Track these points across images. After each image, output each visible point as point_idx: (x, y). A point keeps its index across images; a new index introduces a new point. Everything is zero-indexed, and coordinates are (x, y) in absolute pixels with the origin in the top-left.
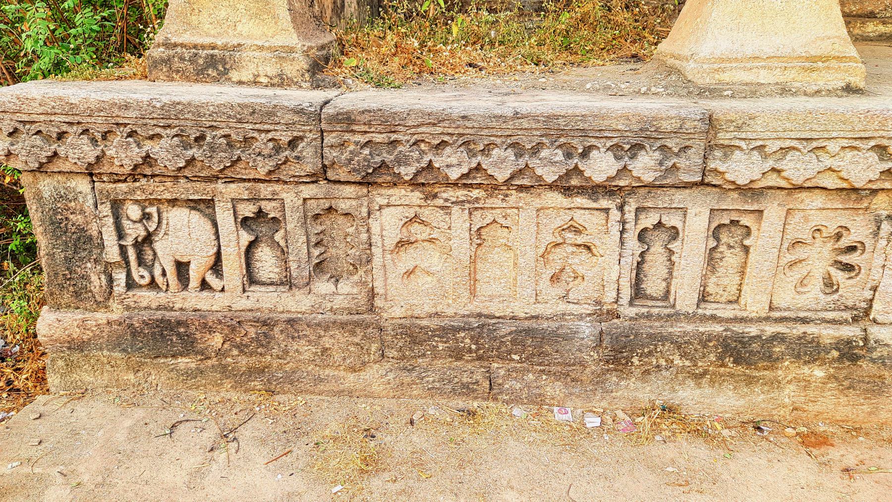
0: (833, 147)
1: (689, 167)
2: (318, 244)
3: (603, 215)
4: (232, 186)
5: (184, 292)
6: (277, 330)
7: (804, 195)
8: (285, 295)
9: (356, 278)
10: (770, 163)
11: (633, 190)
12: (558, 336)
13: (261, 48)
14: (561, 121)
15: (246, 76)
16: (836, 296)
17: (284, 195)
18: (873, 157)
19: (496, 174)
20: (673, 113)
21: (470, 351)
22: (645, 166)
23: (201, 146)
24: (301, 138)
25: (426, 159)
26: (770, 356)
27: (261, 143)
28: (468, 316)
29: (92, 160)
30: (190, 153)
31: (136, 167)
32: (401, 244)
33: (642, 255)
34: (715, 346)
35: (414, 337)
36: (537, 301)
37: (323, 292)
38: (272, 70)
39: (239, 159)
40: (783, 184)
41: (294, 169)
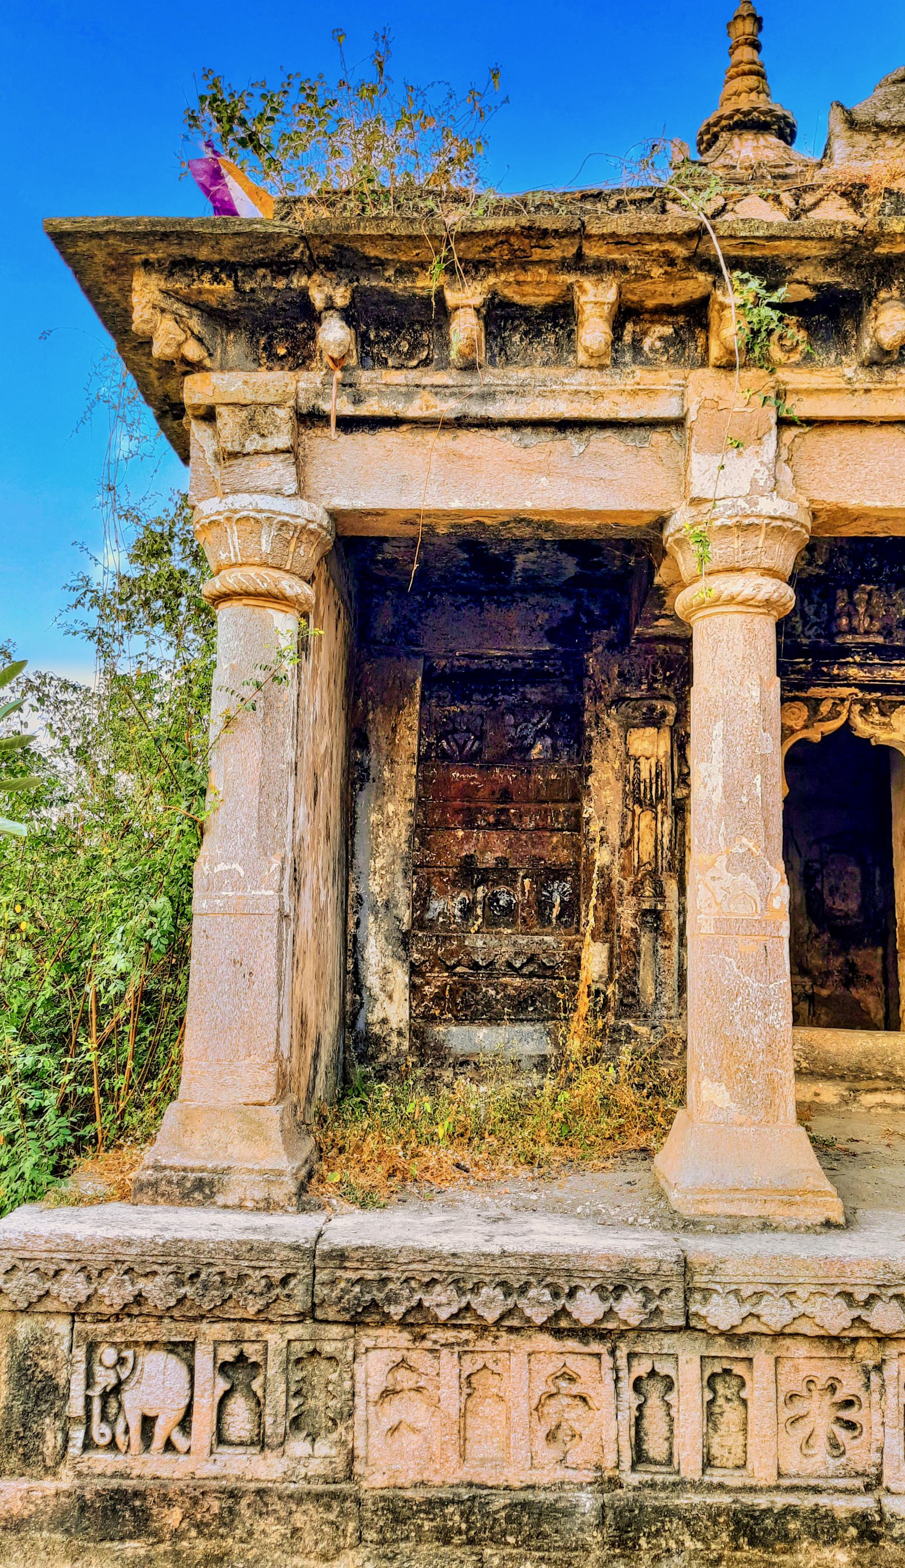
0: (802, 1292)
1: (671, 1309)
2: (298, 1393)
3: (595, 1361)
4: (217, 1326)
5: (145, 1455)
6: (244, 1502)
7: (788, 1342)
8: (254, 1458)
9: (334, 1436)
10: (746, 1309)
11: (622, 1334)
12: (557, 1511)
13: (251, 1171)
14: (546, 1260)
15: (232, 1200)
16: (843, 1460)
17: (267, 1337)
18: (841, 1303)
19: (486, 1315)
20: (649, 1254)
21: (460, 1532)
22: (629, 1308)
23: (193, 1283)
24: (294, 1275)
25: (417, 1297)
26: (786, 1536)
27: (255, 1281)
28: (458, 1486)
29: (83, 1299)
30: (182, 1291)
31: (126, 1305)
32: (388, 1393)
33: (640, 1408)
34: (726, 1523)
35: (397, 1512)
36: (532, 1466)
37: (298, 1454)
38: (259, 1194)
39: (230, 1297)
40: (764, 1330)
41: (286, 1308)
